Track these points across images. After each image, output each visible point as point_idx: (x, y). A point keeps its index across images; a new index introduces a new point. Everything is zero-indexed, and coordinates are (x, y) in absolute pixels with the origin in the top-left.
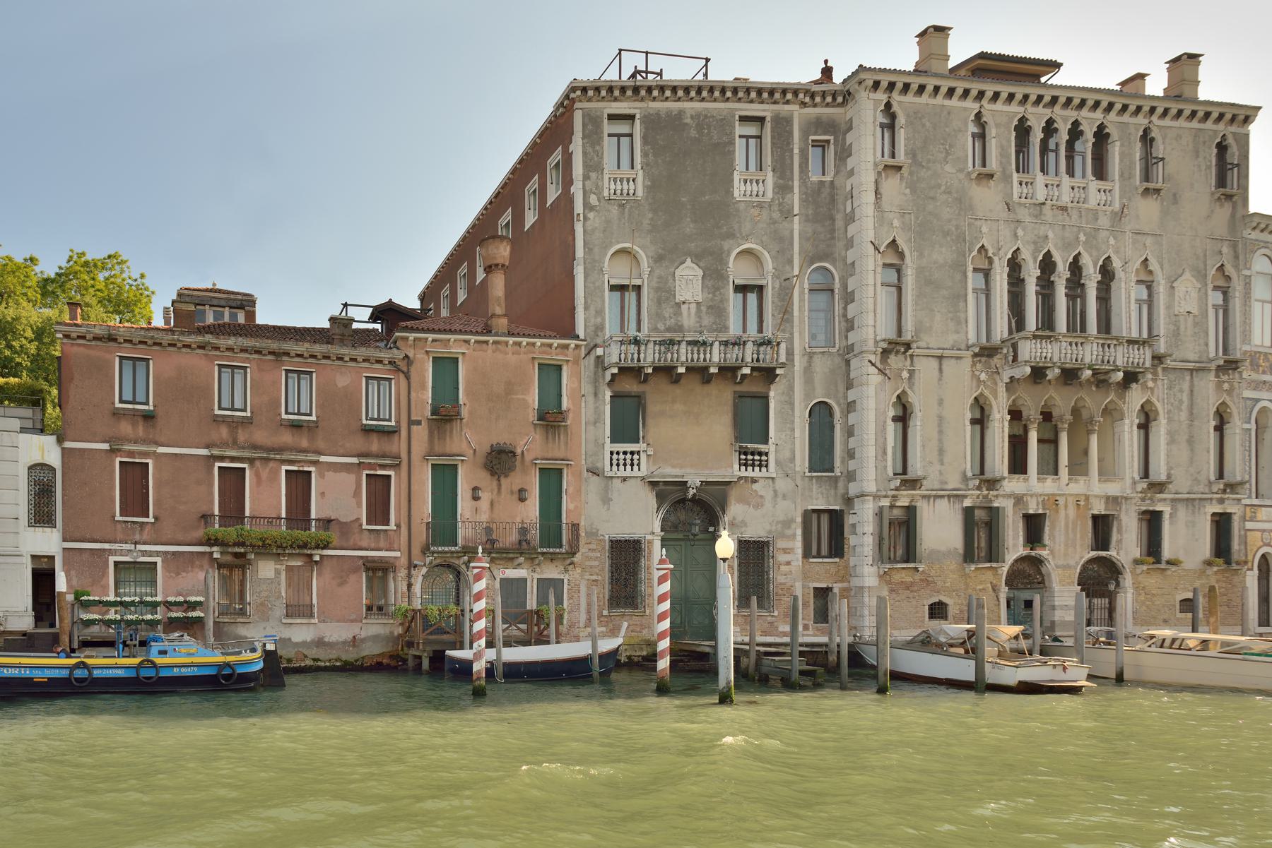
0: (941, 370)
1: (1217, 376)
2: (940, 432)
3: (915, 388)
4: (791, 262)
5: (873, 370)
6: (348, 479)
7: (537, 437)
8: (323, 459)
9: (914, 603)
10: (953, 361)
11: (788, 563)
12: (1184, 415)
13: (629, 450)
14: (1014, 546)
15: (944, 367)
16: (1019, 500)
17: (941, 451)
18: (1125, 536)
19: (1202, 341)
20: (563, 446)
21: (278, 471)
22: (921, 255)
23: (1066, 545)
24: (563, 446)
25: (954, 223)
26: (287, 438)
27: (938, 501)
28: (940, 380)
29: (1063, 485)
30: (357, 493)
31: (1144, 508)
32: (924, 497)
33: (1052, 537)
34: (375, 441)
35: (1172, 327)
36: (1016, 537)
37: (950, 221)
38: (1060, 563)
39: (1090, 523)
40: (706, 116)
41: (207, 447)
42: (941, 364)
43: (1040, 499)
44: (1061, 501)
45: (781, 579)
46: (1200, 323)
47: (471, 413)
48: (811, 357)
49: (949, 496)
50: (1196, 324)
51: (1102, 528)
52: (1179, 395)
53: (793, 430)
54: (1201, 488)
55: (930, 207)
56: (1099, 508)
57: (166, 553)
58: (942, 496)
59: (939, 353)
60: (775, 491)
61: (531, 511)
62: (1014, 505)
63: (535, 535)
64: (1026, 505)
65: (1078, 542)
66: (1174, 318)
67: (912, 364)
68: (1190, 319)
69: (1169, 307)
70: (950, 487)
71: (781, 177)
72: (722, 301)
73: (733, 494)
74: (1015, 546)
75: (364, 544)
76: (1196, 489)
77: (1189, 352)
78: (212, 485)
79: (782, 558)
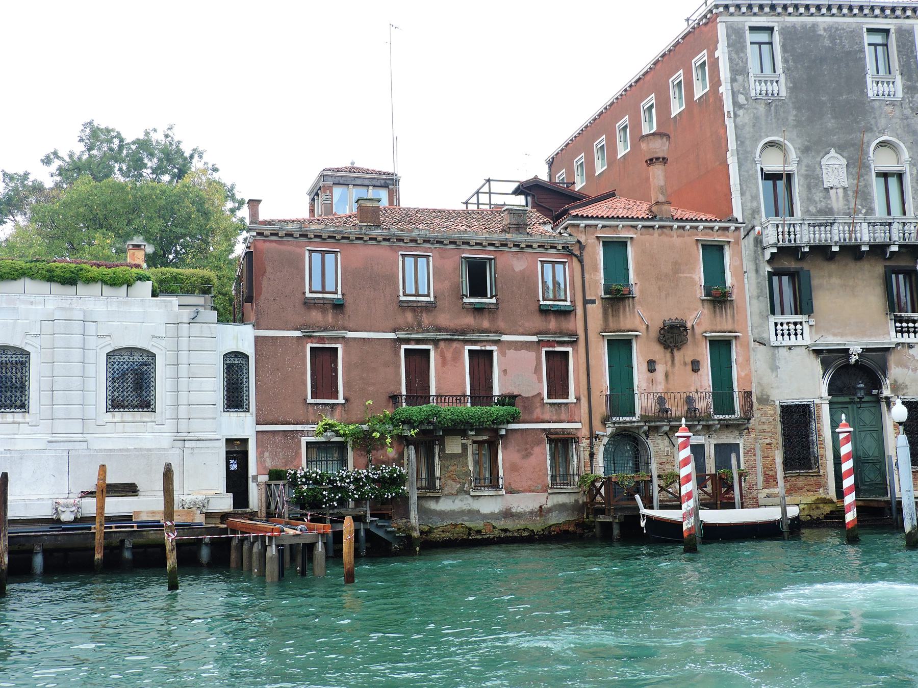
6: (531, 355)
8: (504, 338)
41: (394, 331)
47: (641, 291)
72: (866, 186)
73: (892, 359)
75: (547, 417)
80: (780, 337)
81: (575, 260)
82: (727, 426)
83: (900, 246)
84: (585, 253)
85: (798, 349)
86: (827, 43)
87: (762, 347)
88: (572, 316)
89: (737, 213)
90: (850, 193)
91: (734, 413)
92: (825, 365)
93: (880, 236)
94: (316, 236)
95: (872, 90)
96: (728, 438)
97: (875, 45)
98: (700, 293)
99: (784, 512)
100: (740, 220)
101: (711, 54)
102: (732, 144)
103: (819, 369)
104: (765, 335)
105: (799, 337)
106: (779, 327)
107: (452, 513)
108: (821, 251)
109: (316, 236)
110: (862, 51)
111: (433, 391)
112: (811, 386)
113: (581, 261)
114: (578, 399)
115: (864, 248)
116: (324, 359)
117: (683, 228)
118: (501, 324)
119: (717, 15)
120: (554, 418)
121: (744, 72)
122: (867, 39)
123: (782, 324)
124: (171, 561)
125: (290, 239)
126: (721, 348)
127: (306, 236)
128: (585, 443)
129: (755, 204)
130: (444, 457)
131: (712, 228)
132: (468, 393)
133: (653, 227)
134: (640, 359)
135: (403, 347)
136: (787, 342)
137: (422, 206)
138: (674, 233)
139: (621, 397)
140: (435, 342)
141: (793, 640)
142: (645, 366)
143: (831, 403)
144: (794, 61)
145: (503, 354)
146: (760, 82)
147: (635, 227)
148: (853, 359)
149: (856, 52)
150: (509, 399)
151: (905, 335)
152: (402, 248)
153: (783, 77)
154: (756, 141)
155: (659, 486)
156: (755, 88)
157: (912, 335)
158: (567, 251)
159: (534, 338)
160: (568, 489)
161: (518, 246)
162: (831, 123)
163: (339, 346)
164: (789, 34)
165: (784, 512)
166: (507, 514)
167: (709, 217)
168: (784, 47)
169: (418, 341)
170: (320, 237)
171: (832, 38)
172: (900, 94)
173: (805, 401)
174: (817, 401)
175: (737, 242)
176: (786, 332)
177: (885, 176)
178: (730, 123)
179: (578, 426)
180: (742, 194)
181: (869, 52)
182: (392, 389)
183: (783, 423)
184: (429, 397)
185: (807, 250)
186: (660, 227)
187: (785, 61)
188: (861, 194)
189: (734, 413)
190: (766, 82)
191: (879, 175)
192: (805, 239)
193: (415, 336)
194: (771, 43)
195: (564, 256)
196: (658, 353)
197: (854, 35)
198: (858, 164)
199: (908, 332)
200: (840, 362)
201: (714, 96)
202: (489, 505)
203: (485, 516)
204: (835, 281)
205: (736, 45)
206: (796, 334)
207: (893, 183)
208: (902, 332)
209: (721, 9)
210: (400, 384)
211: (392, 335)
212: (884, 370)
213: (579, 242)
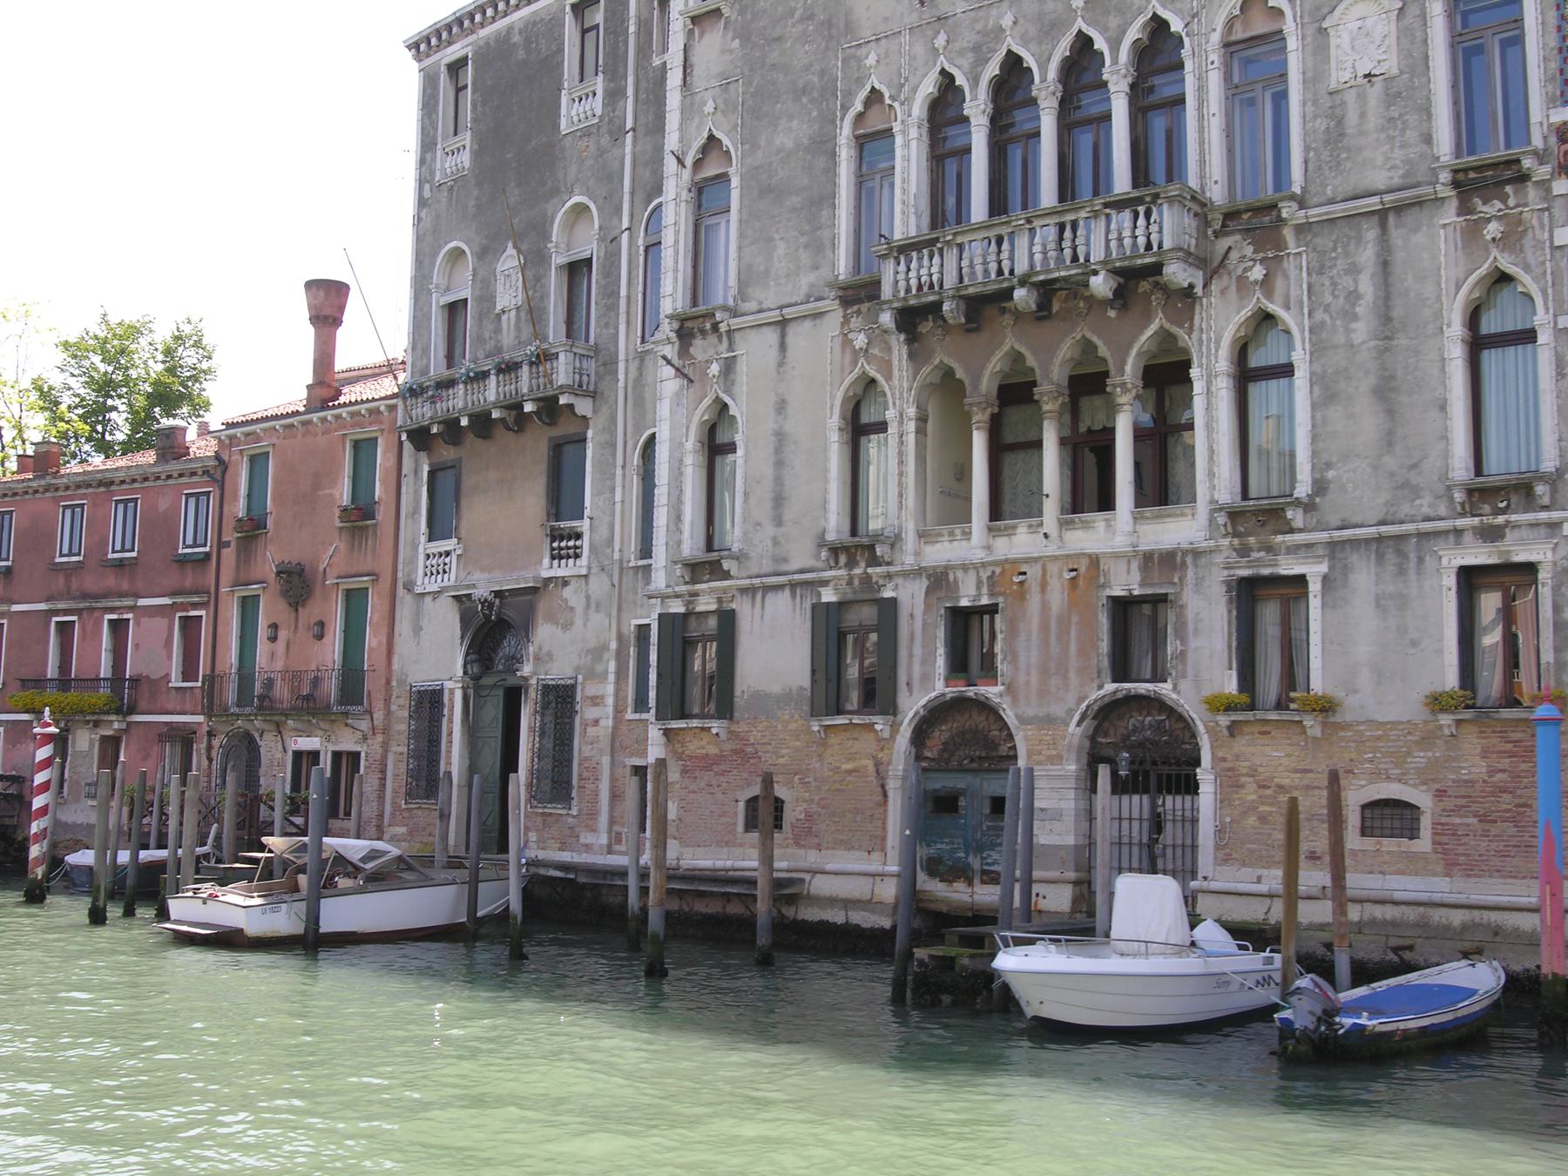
0: (783, 346)
1: (1465, 209)
2: (779, 463)
3: (736, 389)
4: (619, 210)
5: (669, 371)
6: (160, 623)
7: (342, 546)
8: (142, 602)
9: (719, 796)
10: (808, 324)
11: (596, 722)
12: (1362, 330)
13: (442, 549)
14: (925, 679)
15: (790, 340)
16: (939, 580)
17: (779, 500)
18: (1193, 643)
19: (1412, 135)
20: (369, 556)
21: (99, 623)
22: (755, 146)
23: (1044, 672)
24: (369, 556)
25: (817, 67)
26: (110, 581)
27: (770, 597)
28: (781, 364)
29: (1045, 538)
30: (168, 643)
31: (1245, 573)
32: (743, 591)
33: (1012, 655)
34: (190, 572)
35: (1321, 124)
36: (928, 660)
37: (808, 68)
38: (1030, 712)
39: (1104, 621)
40: (535, 24)
41: (47, 600)
42: (783, 336)
43: (984, 575)
44: (1033, 572)
45: (587, 751)
46: (1403, 92)
47: (276, 523)
48: (642, 360)
49: (793, 586)
50: (1391, 97)
51: (1137, 626)
52: (1347, 282)
53: (613, 490)
54: (1424, 505)
55: (774, 57)
56: (1125, 582)
57: (7, 721)
58: (780, 587)
59: (774, 316)
60: (588, 598)
61: (332, 650)
62: (927, 593)
63: (331, 688)
64: (953, 588)
65: (1073, 663)
66: (1326, 102)
67: (731, 348)
68: (1375, 92)
69: (1312, 80)
70: (795, 565)
71: (611, 81)
72: (542, 298)
73: (542, 606)
74: (926, 678)
75: (170, 707)
76: (1405, 509)
77: (1378, 168)
78: (47, 642)
79: (590, 713)
91: (1364, 832)
124: (763, 939)
141: (1341, 1084)
155: (272, 809)
189: (1364, 832)
193: (61, 606)
195: (206, 484)
211: (43, 606)
212: (525, 628)
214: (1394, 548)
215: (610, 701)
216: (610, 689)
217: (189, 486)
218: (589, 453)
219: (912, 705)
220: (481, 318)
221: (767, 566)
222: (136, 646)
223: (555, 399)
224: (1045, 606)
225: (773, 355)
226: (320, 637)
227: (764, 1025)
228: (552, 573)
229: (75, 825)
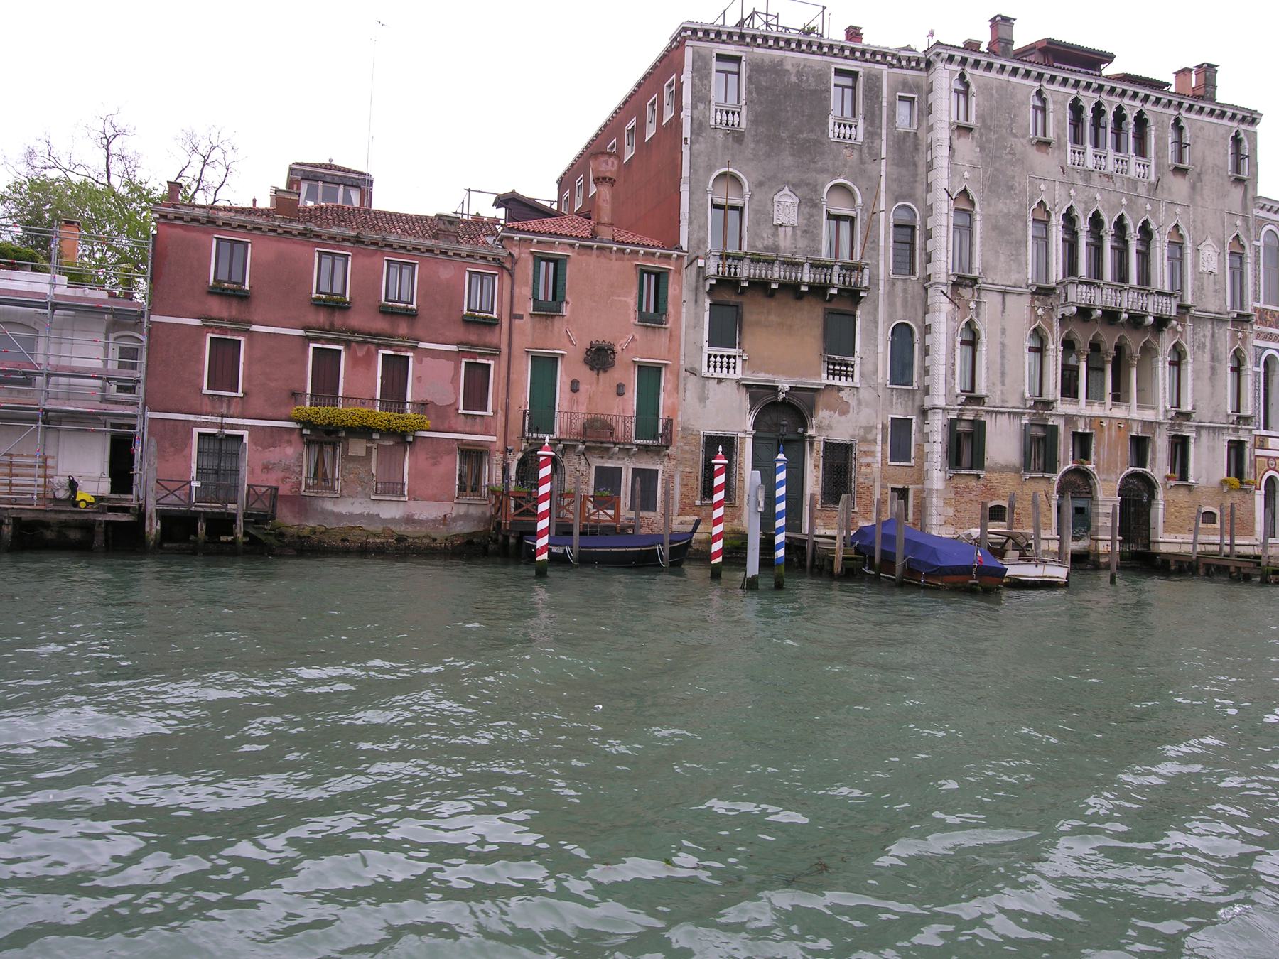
2: (1003, 357)
5: (944, 299)
12: (1207, 357)
14: (1066, 462)
16: (1070, 419)
17: (1003, 374)
32: (987, 412)
49: (1009, 413)
51: (1140, 446)
53: (876, 346)
56: (1136, 431)
58: (1004, 413)
73: (821, 399)
80: (712, 369)
81: (506, 275)
82: (645, 449)
83: (839, 290)
84: (517, 268)
85: (728, 382)
86: (794, 79)
87: (693, 377)
88: (497, 328)
89: (684, 243)
90: (799, 232)
92: (753, 400)
93: (820, 277)
94: (224, 224)
95: (833, 131)
96: (645, 464)
97: (843, 87)
98: (633, 318)
99: (1194, 548)
100: (685, 248)
101: (679, 78)
102: (686, 172)
103: (747, 404)
104: (697, 366)
105: (731, 370)
106: (712, 359)
107: (352, 516)
108: (760, 285)
109: (224, 224)
110: (828, 90)
111: (341, 394)
112: (739, 421)
113: (511, 276)
114: (495, 412)
115: (804, 288)
116: (225, 353)
117: (637, 252)
118: (419, 332)
119: (685, 39)
120: (467, 429)
121: (706, 100)
122: (834, 79)
123: (715, 356)
125: (195, 224)
126: (650, 375)
127: (214, 223)
128: (499, 456)
129: (702, 234)
130: (347, 459)
131: (653, 254)
132: (378, 397)
133: (591, 247)
134: (565, 378)
135: (312, 345)
136: (718, 374)
137: (410, 213)
138: (614, 256)
139: (541, 416)
140: (347, 343)
142: (567, 387)
143: (755, 438)
144: (758, 94)
145: (419, 361)
146: (721, 111)
147: (572, 246)
148: (782, 396)
149: (822, 91)
150: (422, 406)
151: (843, 378)
152: (319, 245)
153: (744, 108)
154: (710, 169)
156: (714, 118)
157: (843, 378)
158: (498, 263)
159: (454, 348)
160: (475, 500)
161: (446, 253)
162: (787, 160)
163: (242, 339)
164: (757, 69)
165: (1194, 548)
166: (409, 520)
167: (656, 243)
168: (749, 78)
169: (329, 341)
170: (230, 225)
171: (799, 74)
172: (860, 138)
173: (729, 434)
174: (741, 435)
175: (679, 272)
176: (718, 364)
177: (838, 218)
178: (686, 150)
179: (494, 439)
180: (690, 223)
181: (835, 93)
182: (296, 386)
183: (825, 458)
184: (405, 403)
185: (746, 284)
186: (598, 248)
187: (749, 92)
188: (809, 231)
190: (727, 113)
191: (831, 217)
192: (745, 274)
194: (738, 73)
195: (493, 268)
196: (584, 374)
197: (821, 77)
198: (810, 203)
199: (840, 375)
200: (770, 399)
201: (676, 122)
202: (390, 511)
203: (385, 520)
204: (774, 318)
205: (701, 72)
206: (728, 368)
207: (845, 226)
208: (834, 375)
209: (689, 33)
210: (305, 381)
212: (812, 410)
213: (511, 255)
214: (1216, 430)
215: (879, 454)
216: (879, 449)
217: (472, 265)
218: (858, 323)
219: (1063, 469)
220: (757, 223)
221: (998, 403)
222: (418, 379)
223: (859, 292)
224: (1110, 436)
225: (1000, 307)
226: (620, 394)
227: (343, 561)
228: (828, 383)
229: (352, 515)
